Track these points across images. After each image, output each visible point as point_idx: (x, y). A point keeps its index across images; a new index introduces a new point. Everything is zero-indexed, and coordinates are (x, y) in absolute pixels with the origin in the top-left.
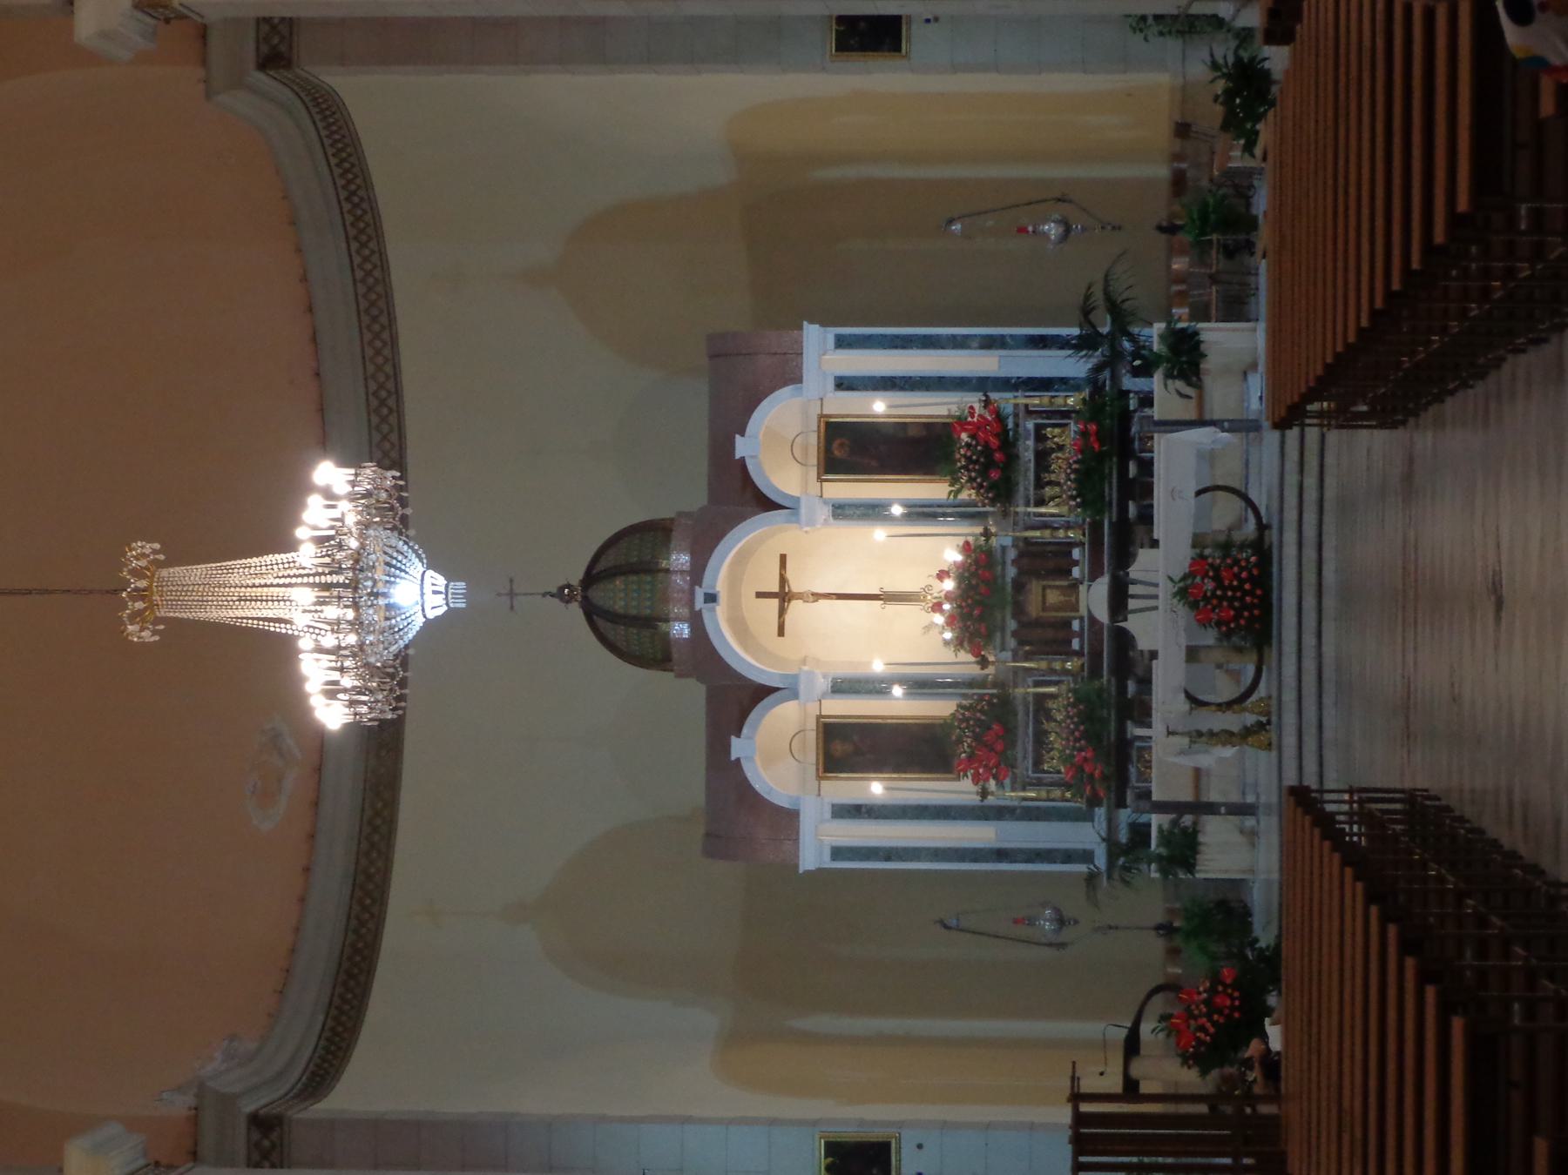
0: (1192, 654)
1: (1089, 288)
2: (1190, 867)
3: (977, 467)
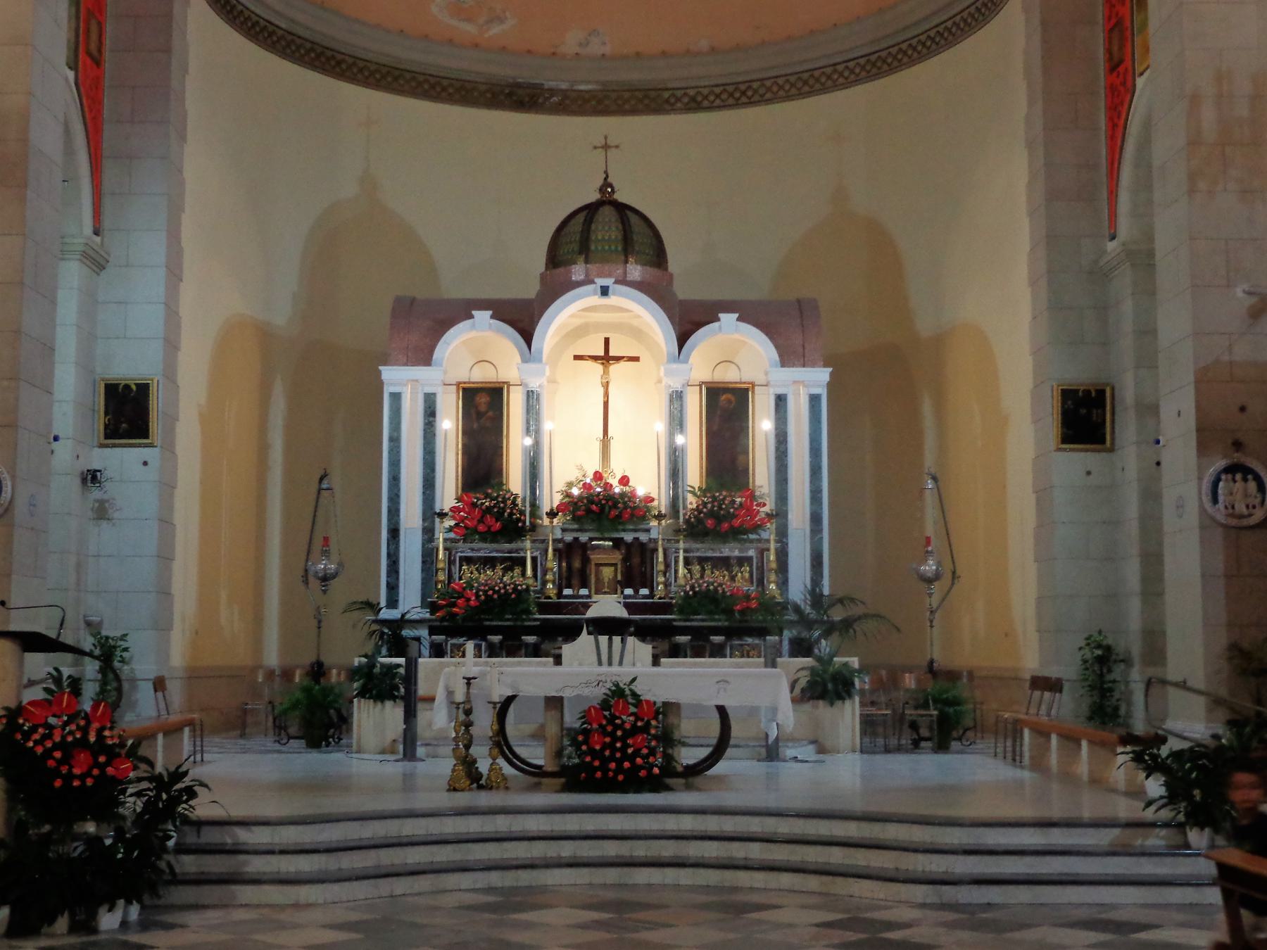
0: (555, 703)
2: (362, 694)
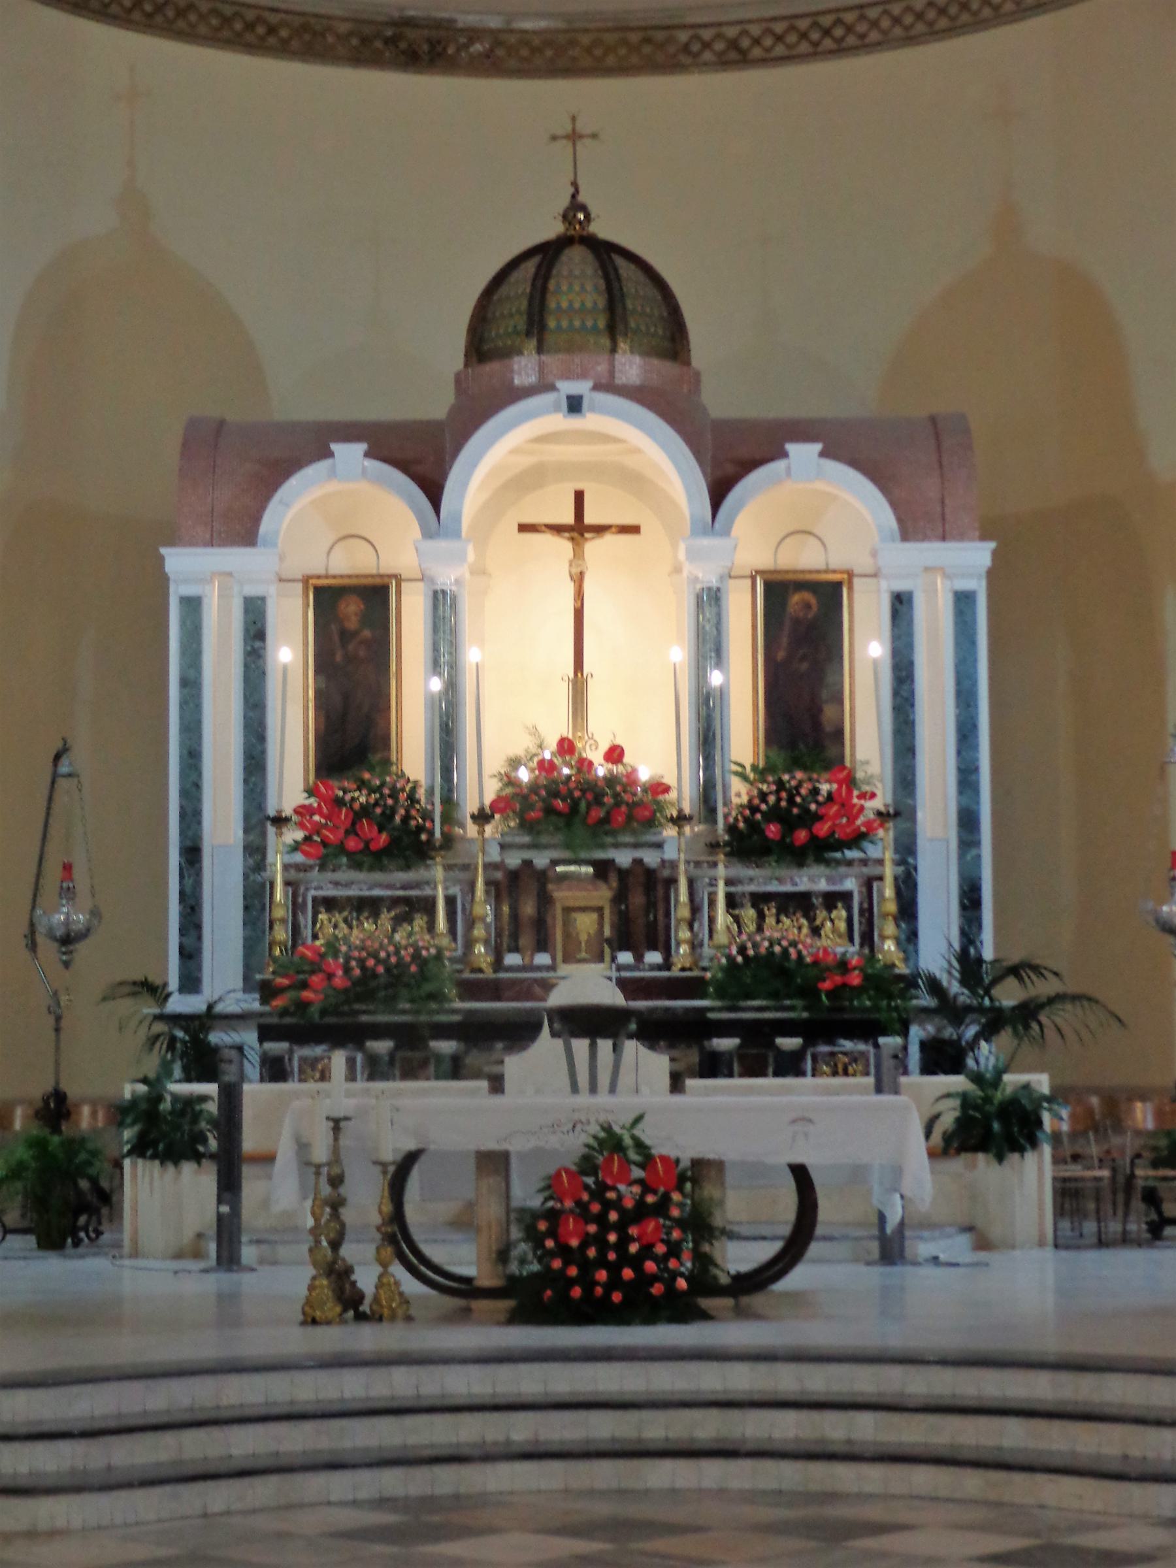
1: (1056, 974)
2: (140, 1149)
3: (783, 804)
